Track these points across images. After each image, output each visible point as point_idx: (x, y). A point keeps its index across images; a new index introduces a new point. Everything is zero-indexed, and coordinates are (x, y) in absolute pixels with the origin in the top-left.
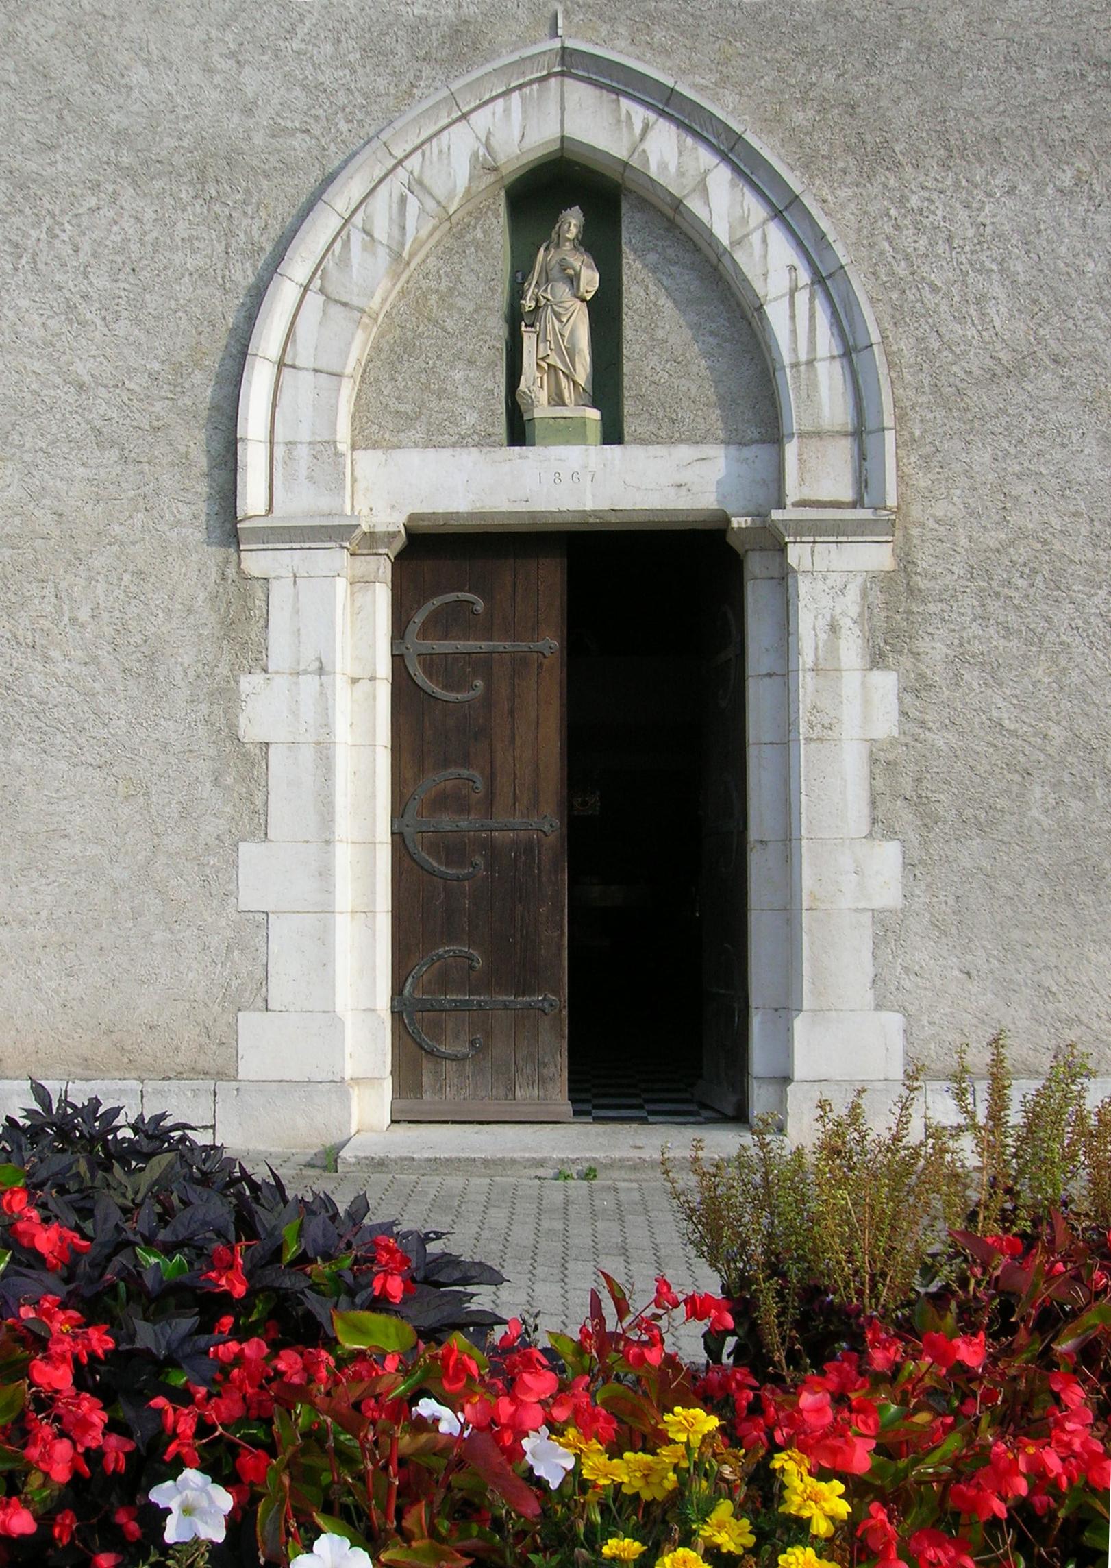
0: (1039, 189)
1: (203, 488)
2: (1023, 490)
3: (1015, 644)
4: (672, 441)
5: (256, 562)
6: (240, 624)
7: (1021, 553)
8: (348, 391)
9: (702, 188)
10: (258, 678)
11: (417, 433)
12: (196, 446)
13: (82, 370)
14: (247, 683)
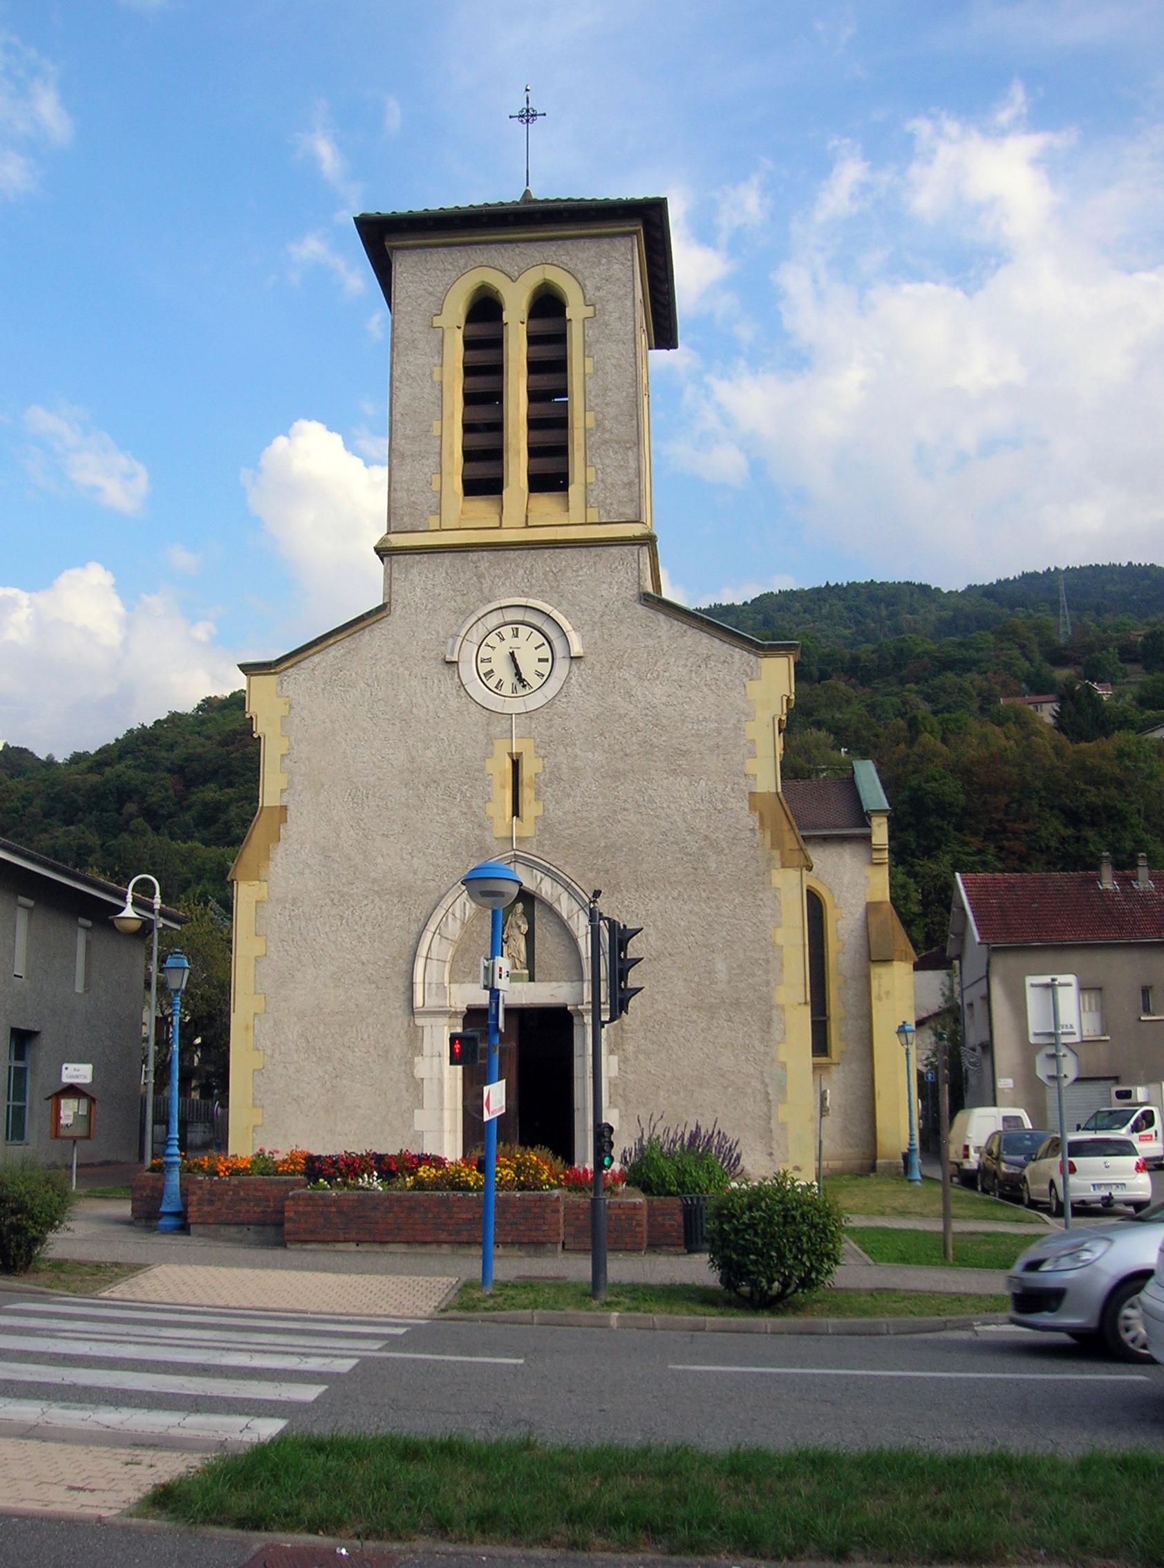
0: (666, 897)
1: (402, 997)
2: (659, 997)
3: (655, 1047)
4: (551, 981)
5: (420, 1021)
6: (414, 1040)
7: (658, 1017)
8: (447, 967)
9: (559, 900)
10: (420, 1058)
11: (470, 979)
12: (401, 984)
13: (364, 958)
14: (416, 1059)
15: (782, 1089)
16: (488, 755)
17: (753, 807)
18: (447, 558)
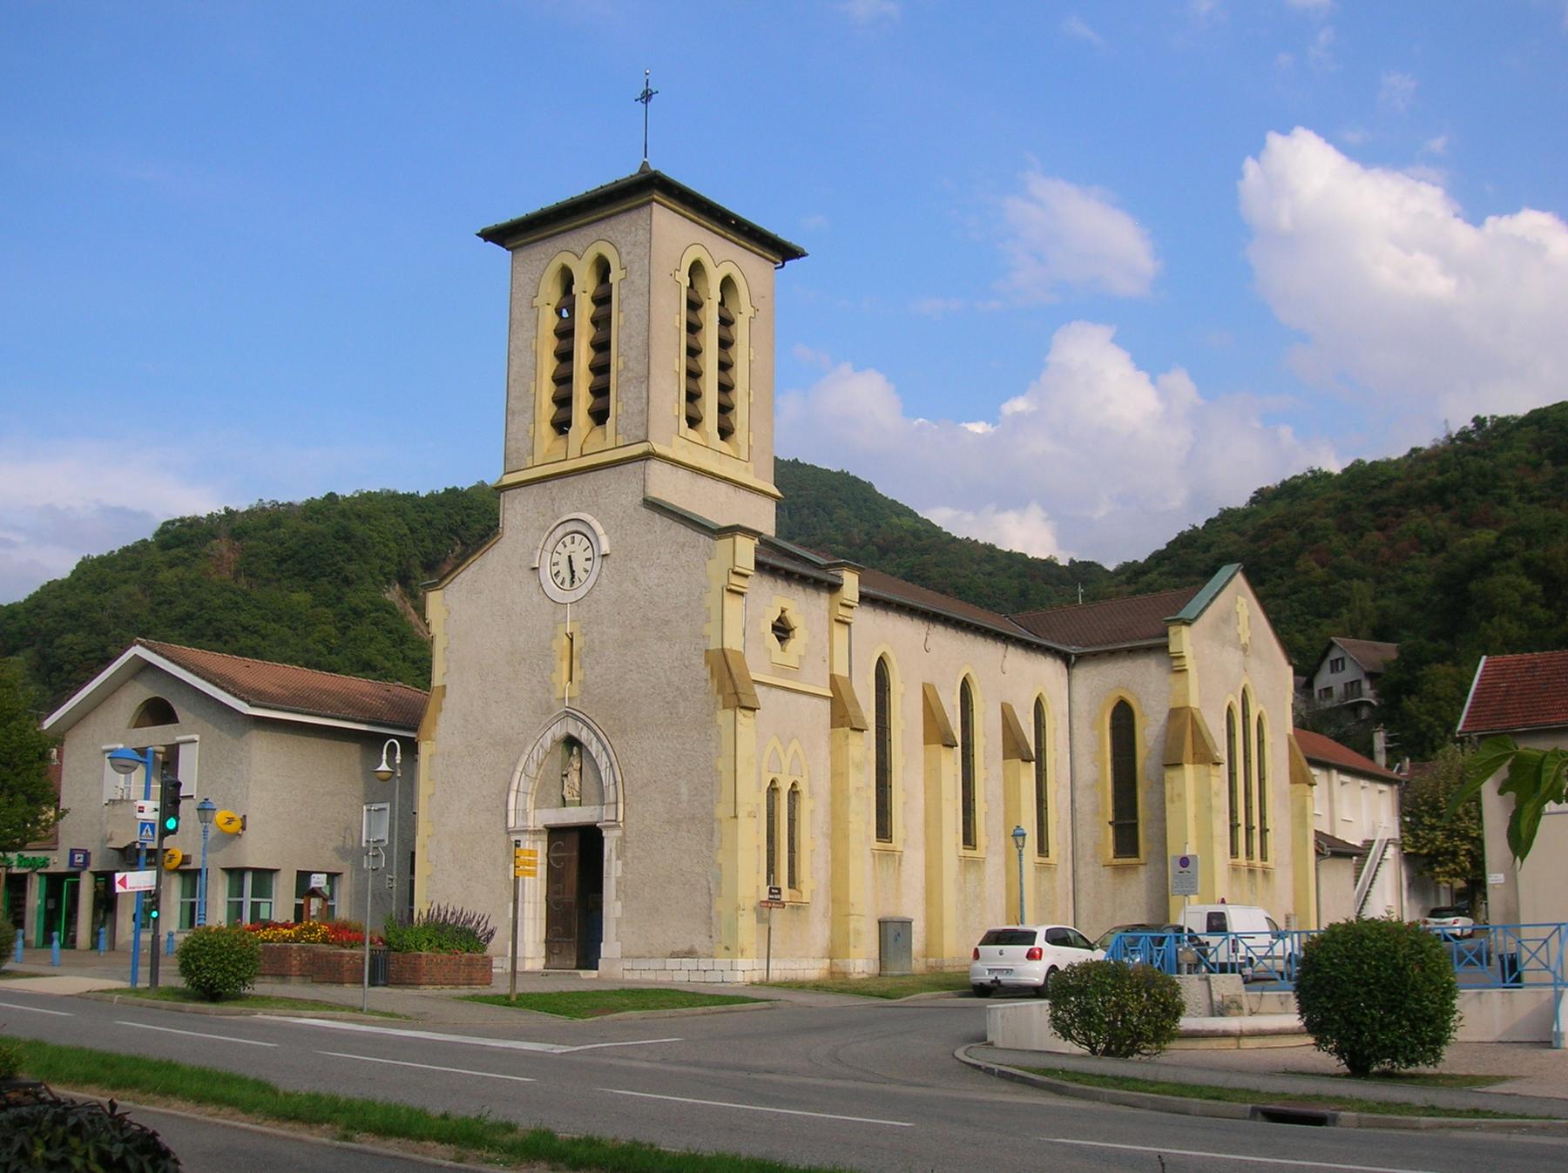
15: (719, 884)
16: (554, 637)
17: (707, 662)
18: (535, 488)
